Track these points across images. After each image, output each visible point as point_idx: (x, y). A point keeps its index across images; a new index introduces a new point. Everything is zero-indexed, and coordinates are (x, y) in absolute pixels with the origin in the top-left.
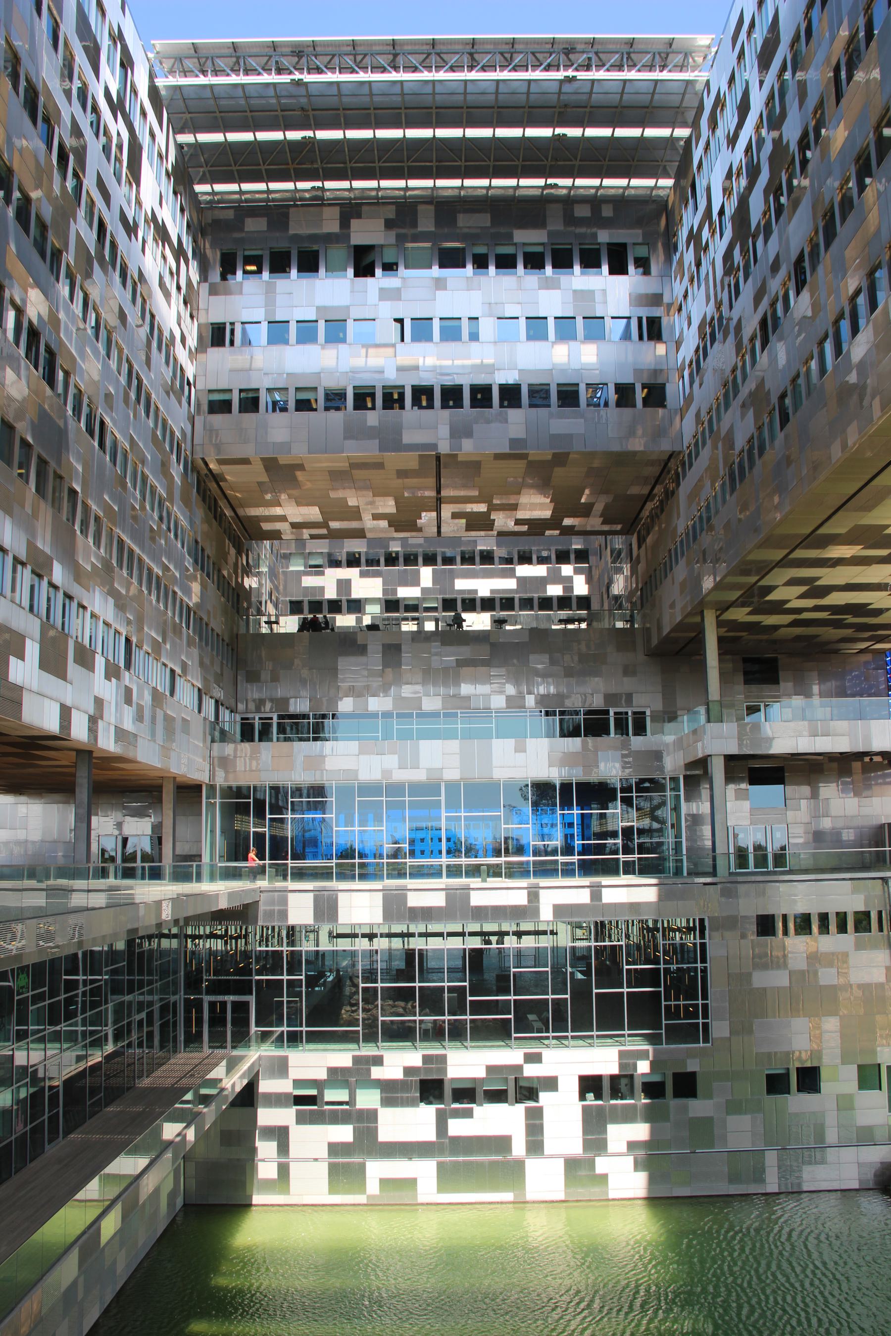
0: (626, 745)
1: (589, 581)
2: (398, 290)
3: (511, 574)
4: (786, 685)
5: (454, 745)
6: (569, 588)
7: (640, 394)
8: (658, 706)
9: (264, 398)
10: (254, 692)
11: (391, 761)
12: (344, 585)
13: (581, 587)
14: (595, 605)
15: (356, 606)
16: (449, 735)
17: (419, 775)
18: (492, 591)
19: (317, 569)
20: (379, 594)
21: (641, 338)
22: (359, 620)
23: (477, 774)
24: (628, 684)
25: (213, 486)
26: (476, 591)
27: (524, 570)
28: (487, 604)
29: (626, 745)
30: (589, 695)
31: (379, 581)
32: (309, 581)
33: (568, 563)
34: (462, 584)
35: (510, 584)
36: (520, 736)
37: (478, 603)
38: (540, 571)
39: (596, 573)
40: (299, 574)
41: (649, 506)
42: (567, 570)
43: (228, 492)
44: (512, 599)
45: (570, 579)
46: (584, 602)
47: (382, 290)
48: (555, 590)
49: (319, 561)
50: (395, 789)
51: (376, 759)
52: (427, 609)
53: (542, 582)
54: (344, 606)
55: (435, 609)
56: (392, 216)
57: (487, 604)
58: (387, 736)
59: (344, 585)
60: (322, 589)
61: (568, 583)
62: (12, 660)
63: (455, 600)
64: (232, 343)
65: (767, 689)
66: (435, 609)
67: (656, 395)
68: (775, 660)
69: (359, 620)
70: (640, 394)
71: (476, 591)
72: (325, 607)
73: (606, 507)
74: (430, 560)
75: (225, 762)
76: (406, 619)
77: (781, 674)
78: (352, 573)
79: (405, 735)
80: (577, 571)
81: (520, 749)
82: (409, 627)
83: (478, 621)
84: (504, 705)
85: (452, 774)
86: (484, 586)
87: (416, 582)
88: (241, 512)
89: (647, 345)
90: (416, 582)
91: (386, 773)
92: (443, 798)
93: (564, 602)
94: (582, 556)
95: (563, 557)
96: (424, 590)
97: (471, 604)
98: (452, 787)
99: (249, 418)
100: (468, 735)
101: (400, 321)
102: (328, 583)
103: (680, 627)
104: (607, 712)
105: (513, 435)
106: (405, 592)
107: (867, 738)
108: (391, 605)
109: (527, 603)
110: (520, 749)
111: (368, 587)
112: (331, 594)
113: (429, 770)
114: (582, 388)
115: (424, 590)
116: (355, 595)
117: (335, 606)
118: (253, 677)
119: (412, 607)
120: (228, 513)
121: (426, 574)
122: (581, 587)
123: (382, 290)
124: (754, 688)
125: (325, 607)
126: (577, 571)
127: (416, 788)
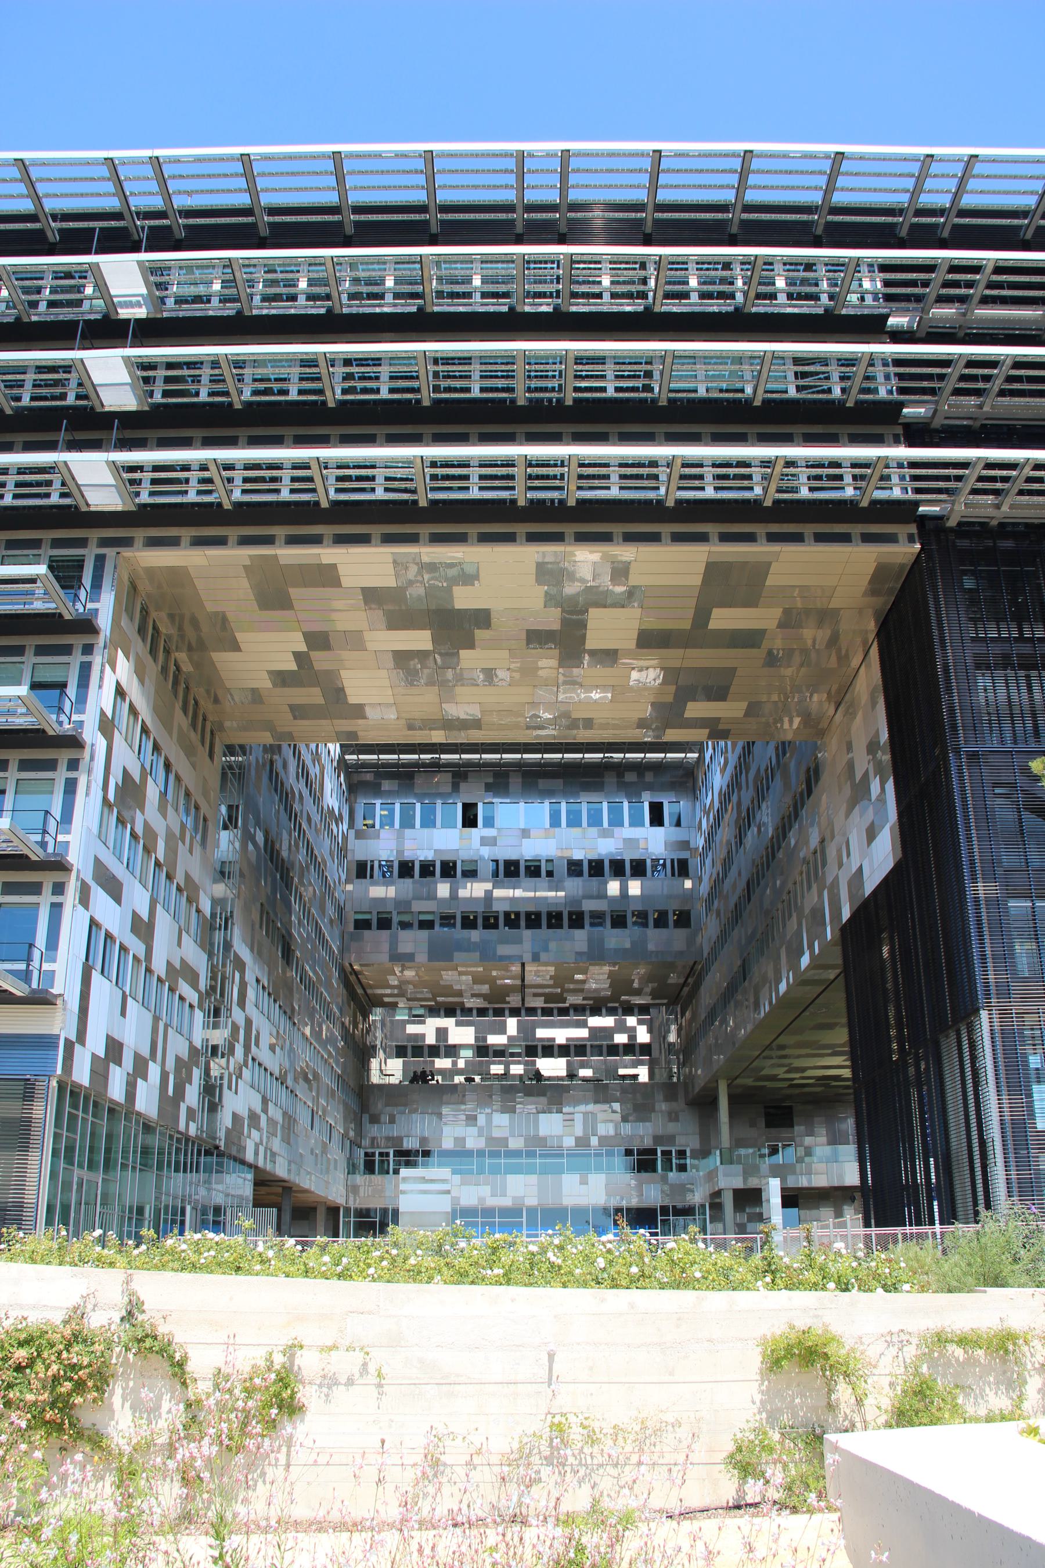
0: (664, 1179)
1: (650, 1031)
2: (495, 838)
3: (583, 1024)
4: (799, 1129)
5: (533, 1179)
6: (633, 1037)
7: (672, 918)
8: (697, 1145)
9: (395, 919)
10: (374, 1131)
11: (485, 1191)
12: (442, 1033)
13: (643, 1036)
14: (655, 1053)
15: (452, 1051)
16: (530, 1170)
17: (506, 1202)
18: (568, 1039)
19: (419, 1019)
20: (471, 1041)
21: (673, 875)
22: (455, 1063)
23: (550, 1201)
24: (672, 1128)
25: (353, 978)
26: (553, 1039)
27: (595, 1021)
28: (564, 1051)
29: (664, 1179)
30: (643, 1133)
31: (472, 1029)
32: (412, 1029)
33: (632, 1015)
34: (541, 1033)
35: (583, 1033)
36: (584, 1171)
37: (556, 1050)
38: (608, 1021)
39: (656, 1024)
40: (404, 1023)
41: (686, 989)
42: (631, 1021)
43: (364, 981)
44: (585, 1046)
45: (633, 1029)
46: (645, 1049)
47: (482, 838)
48: (621, 1039)
49: (421, 1012)
50: (488, 1212)
51: (473, 1188)
52: (512, 1055)
53: (608, 1032)
54: (442, 1051)
55: (519, 1055)
56: (491, 780)
57: (564, 1051)
58: (481, 1172)
59: (442, 1033)
60: (423, 1036)
61: (632, 1033)
62: (139, 1080)
63: (536, 1047)
64: (372, 877)
65: (785, 1133)
66: (519, 1055)
67: (684, 919)
68: (790, 1107)
69: (455, 1063)
70: (672, 918)
71: (553, 1039)
72: (426, 1051)
73: (653, 989)
74: (515, 1012)
75: (354, 1189)
76: (494, 1063)
77: (795, 1119)
78: (449, 1023)
79: (495, 1170)
80: (640, 1022)
81: (584, 1182)
82: (497, 1069)
83: (552, 1067)
84: (573, 1144)
85: (532, 1201)
86: (561, 1035)
87: (502, 1030)
88: (369, 991)
89: (677, 881)
90: (502, 1030)
91: (482, 1199)
92: (524, 1220)
93: (630, 1048)
94: (643, 1010)
95: (629, 1010)
96: (510, 1038)
97: (549, 1050)
98: (532, 1211)
99: (385, 933)
100: (544, 1171)
101: (497, 861)
102: (428, 1029)
103: (704, 1089)
104: (654, 1152)
105: (578, 950)
106: (493, 1040)
107: (841, 1176)
108: (482, 1050)
109: (598, 1050)
110: (584, 1182)
111: (462, 1034)
112: (431, 1040)
113: (514, 1198)
114: (649, 863)
115: (510, 1038)
116: (451, 1041)
117: (434, 1051)
118: (375, 1119)
119: (500, 1053)
120: (360, 991)
121: (512, 1024)
122: (643, 1036)
123: (482, 838)
124: (773, 1130)
125: (426, 1051)
126: (640, 1022)
127: (505, 1212)
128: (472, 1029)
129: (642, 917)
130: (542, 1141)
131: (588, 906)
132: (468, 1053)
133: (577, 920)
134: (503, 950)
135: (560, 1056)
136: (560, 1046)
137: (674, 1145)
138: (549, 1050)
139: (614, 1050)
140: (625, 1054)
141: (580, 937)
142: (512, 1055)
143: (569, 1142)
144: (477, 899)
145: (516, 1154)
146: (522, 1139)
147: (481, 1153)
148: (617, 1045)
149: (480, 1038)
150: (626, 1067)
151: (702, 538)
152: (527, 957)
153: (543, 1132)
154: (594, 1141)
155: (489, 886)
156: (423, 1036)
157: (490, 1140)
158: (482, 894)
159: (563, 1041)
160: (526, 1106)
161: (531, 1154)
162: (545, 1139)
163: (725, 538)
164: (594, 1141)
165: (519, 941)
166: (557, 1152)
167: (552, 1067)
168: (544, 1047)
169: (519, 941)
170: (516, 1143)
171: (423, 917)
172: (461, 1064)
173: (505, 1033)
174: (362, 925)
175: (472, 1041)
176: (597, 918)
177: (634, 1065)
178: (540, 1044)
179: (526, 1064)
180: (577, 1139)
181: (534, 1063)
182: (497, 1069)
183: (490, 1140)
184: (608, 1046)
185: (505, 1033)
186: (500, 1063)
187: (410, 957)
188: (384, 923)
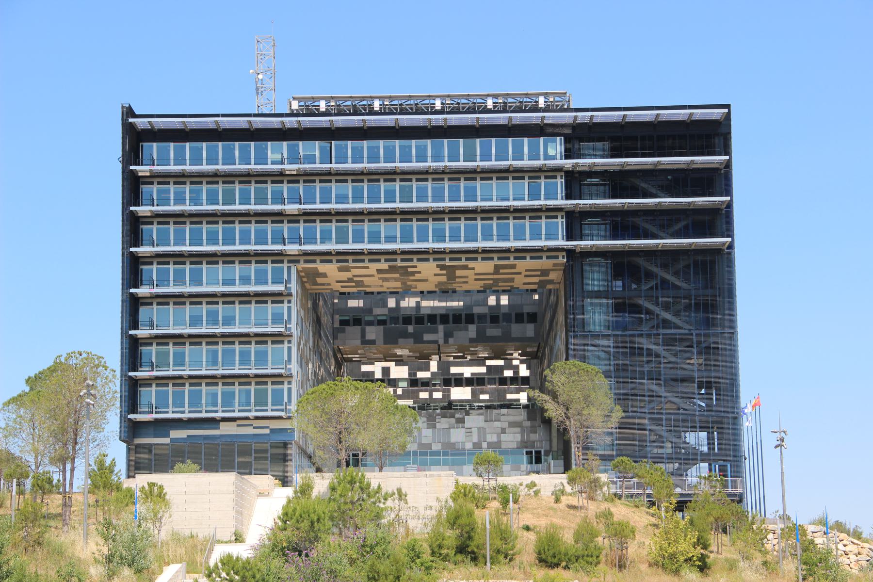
12: (386, 371)
15: (393, 383)
22: (395, 391)
26: (462, 374)
28: (469, 382)
31: (406, 368)
34: (454, 370)
35: (482, 370)
44: (484, 379)
46: (525, 380)
48: (508, 373)
53: (500, 369)
57: (469, 382)
59: (386, 371)
60: (373, 373)
61: (516, 369)
63: (450, 379)
69: (395, 391)
71: (462, 374)
76: (422, 391)
78: (391, 364)
80: (522, 362)
82: (424, 395)
83: (460, 393)
86: (467, 372)
87: (427, 368)
90: (427, 368)
93: (515, 379)
106: (421, 375)
108: (414, 382)
109: (492, 381)
116: (392, 376)
119: (425, 384)
122: (524, 371)
128: (406, 368)
129: (507, 317)
130: (452, 445)
131: (477, 310)
132: (404, 384)
133: (470, 318)
134: (427, 337)
135: (467, 385)
136: (467, 379)
137: (534, 447)
138: (460, 381)
139: (503, 381)
140: (511, 384)
141: (472, 330)
142: (434, 385)
143: (469, 446)
144: (412, 308)
145: (437, 453)
146: (440, 445)
147: (415, 453)
148: (506, 378)
149: (412, 374)
150: (511, 393)
151: (492, 259)
152: (441, 341)
153: (453, 440)
154: (485, 445)
155: (419, 299)
156: (373, 373)
157: (421, 445)
158: (414, 305)
159: (469, 376)
160: (443, 423)
161: (445, 454)
162: (454, 444)
163: (499, 259)
164: (485, 445)
165: (436, 331)
166: (461, 452)
167: (460, 393)
168: (456, 380)
169: (436, 331)
170: (436, 447)
171: (379, 318)
172: (399, 392)
173: (429, 370)
174: (344, 323)
175: (407, 376)
176: (482, 317)
177: (518, 391)
178: (453, 378)
179: (443, 391)
180: (474, 444)
181: (449, 391)
182: (424, 395)
183: (421, 445)
184: (500, 379)
185: (429, 370)
186: (426, 391)
187: (373, 342)
188: (357, 322)
